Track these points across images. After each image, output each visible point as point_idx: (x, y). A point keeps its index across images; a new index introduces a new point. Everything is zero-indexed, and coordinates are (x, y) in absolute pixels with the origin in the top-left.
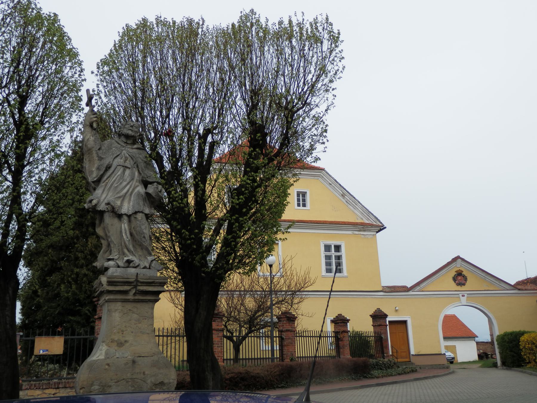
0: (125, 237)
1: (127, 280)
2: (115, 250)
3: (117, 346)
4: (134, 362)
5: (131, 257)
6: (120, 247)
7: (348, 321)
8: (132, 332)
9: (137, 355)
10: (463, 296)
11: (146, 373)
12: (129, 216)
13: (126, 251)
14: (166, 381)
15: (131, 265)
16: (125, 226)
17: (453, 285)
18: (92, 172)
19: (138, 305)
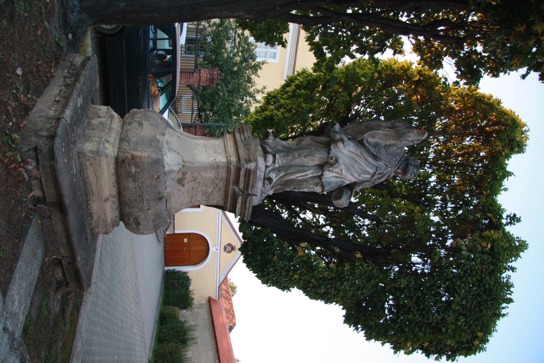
0: (298, 175)
2: (284, 161)
3: (178, 179)
4: (160, 199)
8: (193, 189)
9: (168, 199)
10: (216, 250)
11: (149, 211)
12: (320, 177)
14: (140, 227)
15: (267, 182)
17: (225, 243)
18: (374, 137)
19: (222, 192)
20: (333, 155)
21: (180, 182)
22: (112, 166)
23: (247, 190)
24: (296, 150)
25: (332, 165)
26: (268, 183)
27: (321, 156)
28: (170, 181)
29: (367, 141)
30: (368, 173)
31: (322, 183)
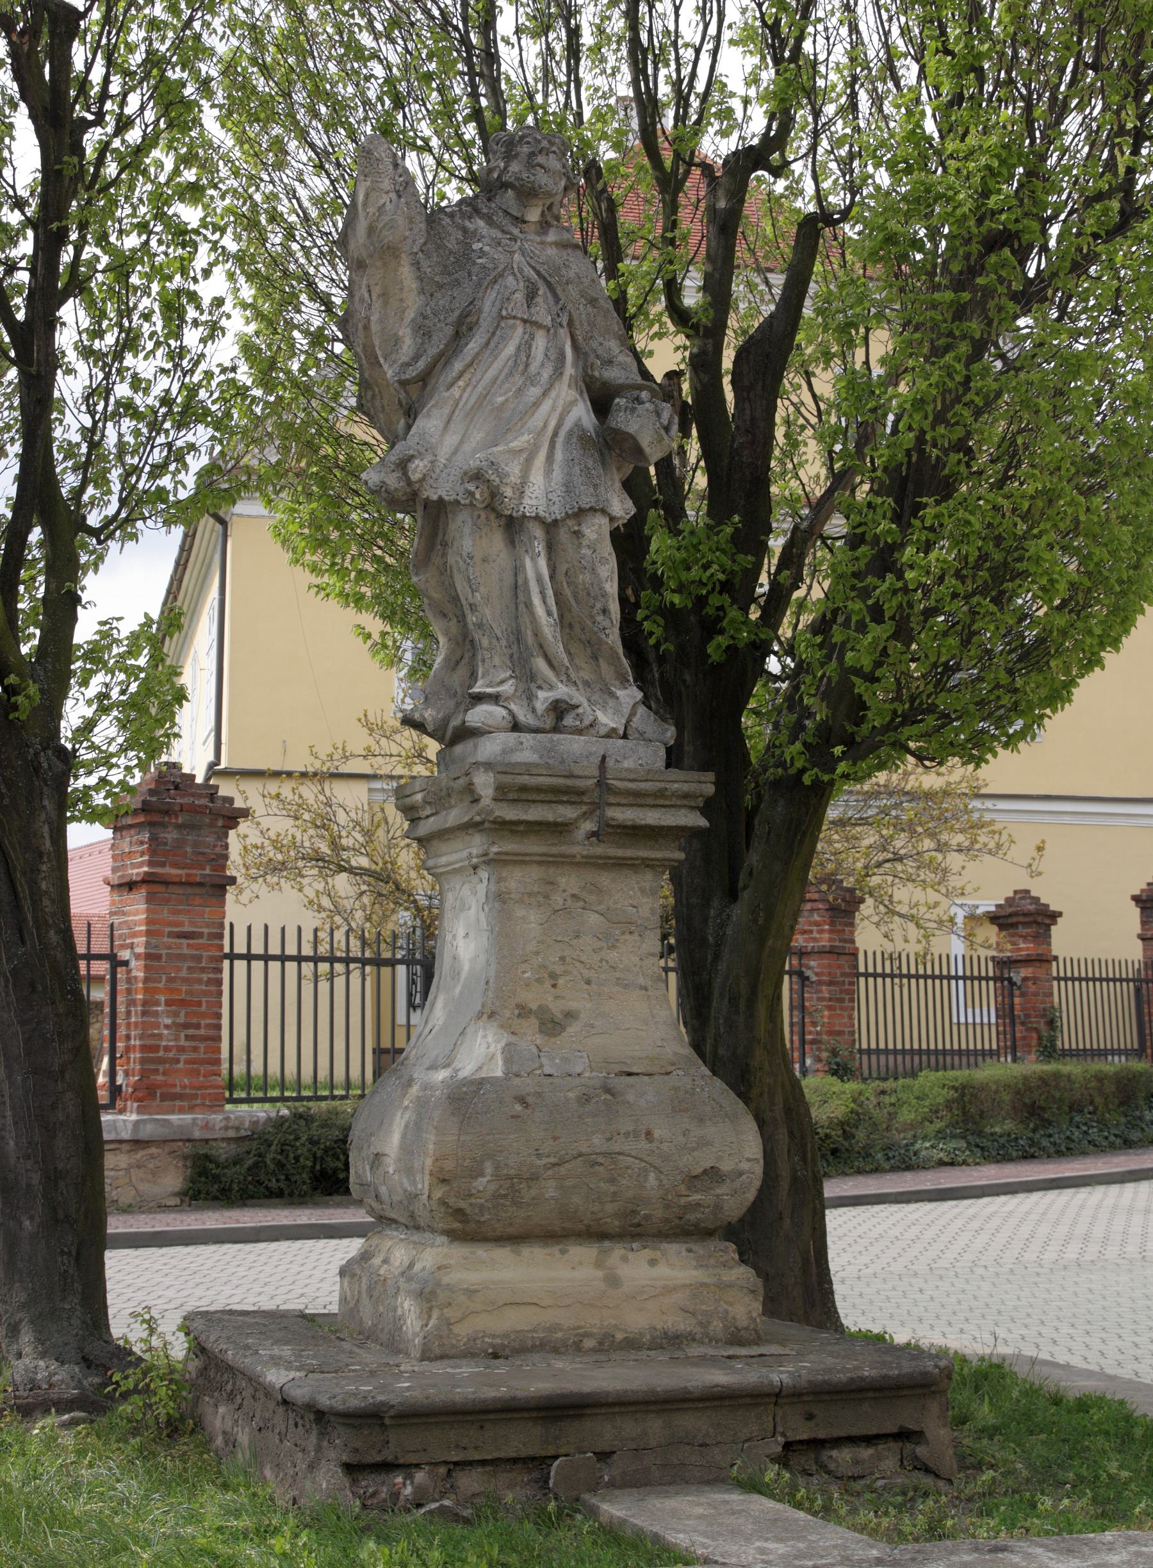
0: (540, 610)
1: (569, 782)
2: (497, 661)
3: (541, 1031)
5: (562, 691)
6: (515, 647)
7: (1054, 916)
8: (588, 982)
9: (618, 1068)
11: (657, 1134)
12: (551, 527)
13: (540, 664)
14: (726, 1166)
15: (569, 721)
16: (536, 566)
18: (397, 341)
19: (605, 879)
20: (461, 490)
21: (552, 1025)
22: (481, 1252)
23: (581, 793)
24: (462, 619)
25: (494, 494)
26: (572, 715)
27: (467, 530)
28: (544, 1061)
29: (416, 358)
30: (526, 347)
31: (568, 516)
